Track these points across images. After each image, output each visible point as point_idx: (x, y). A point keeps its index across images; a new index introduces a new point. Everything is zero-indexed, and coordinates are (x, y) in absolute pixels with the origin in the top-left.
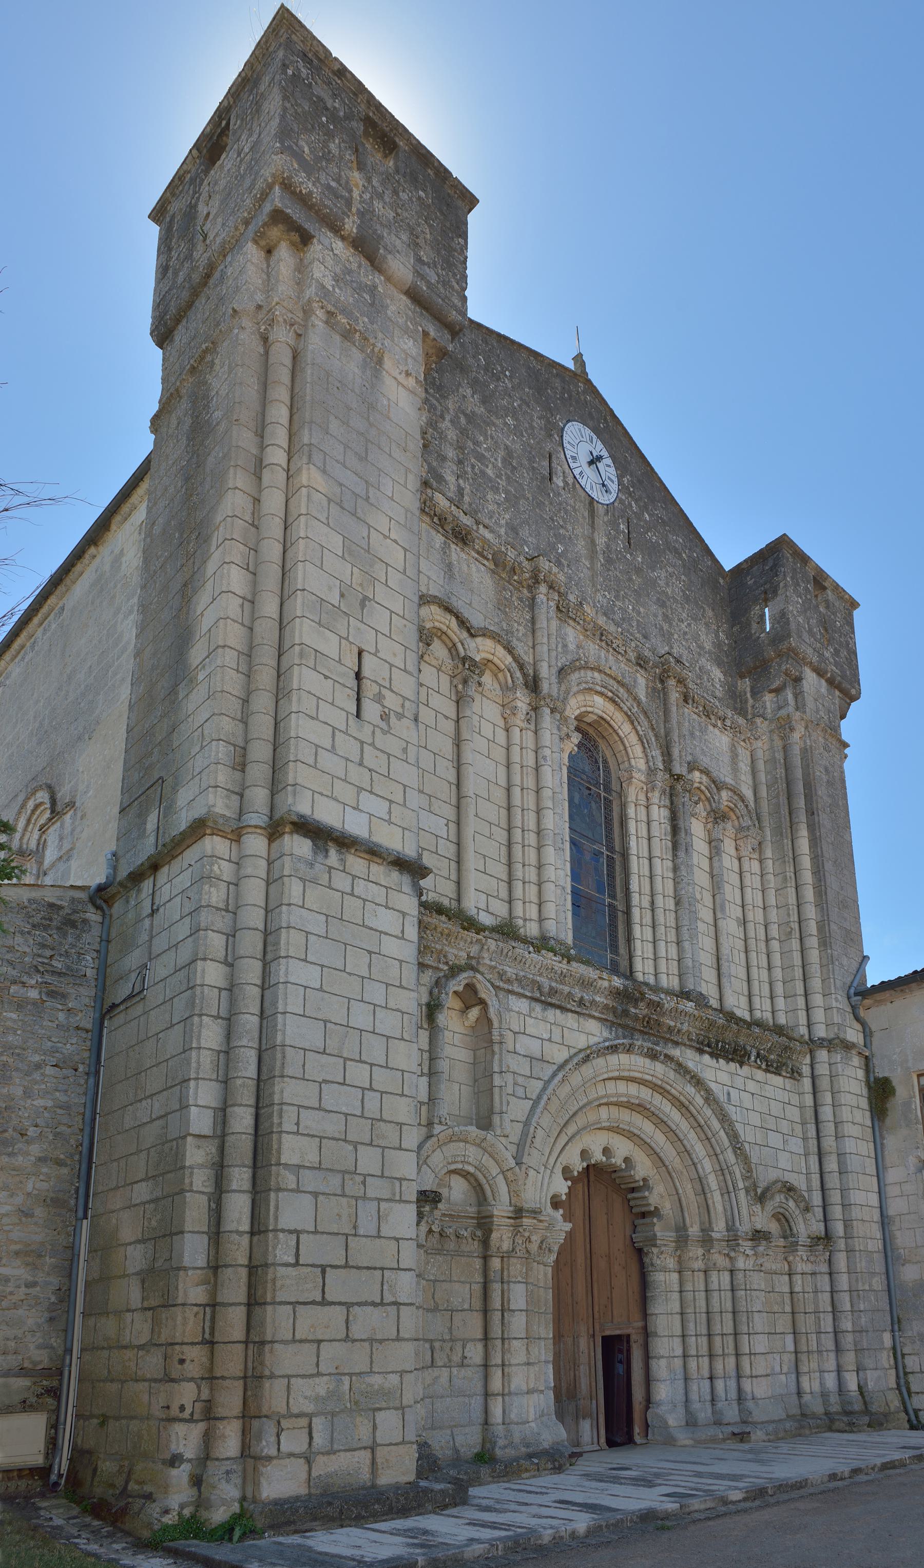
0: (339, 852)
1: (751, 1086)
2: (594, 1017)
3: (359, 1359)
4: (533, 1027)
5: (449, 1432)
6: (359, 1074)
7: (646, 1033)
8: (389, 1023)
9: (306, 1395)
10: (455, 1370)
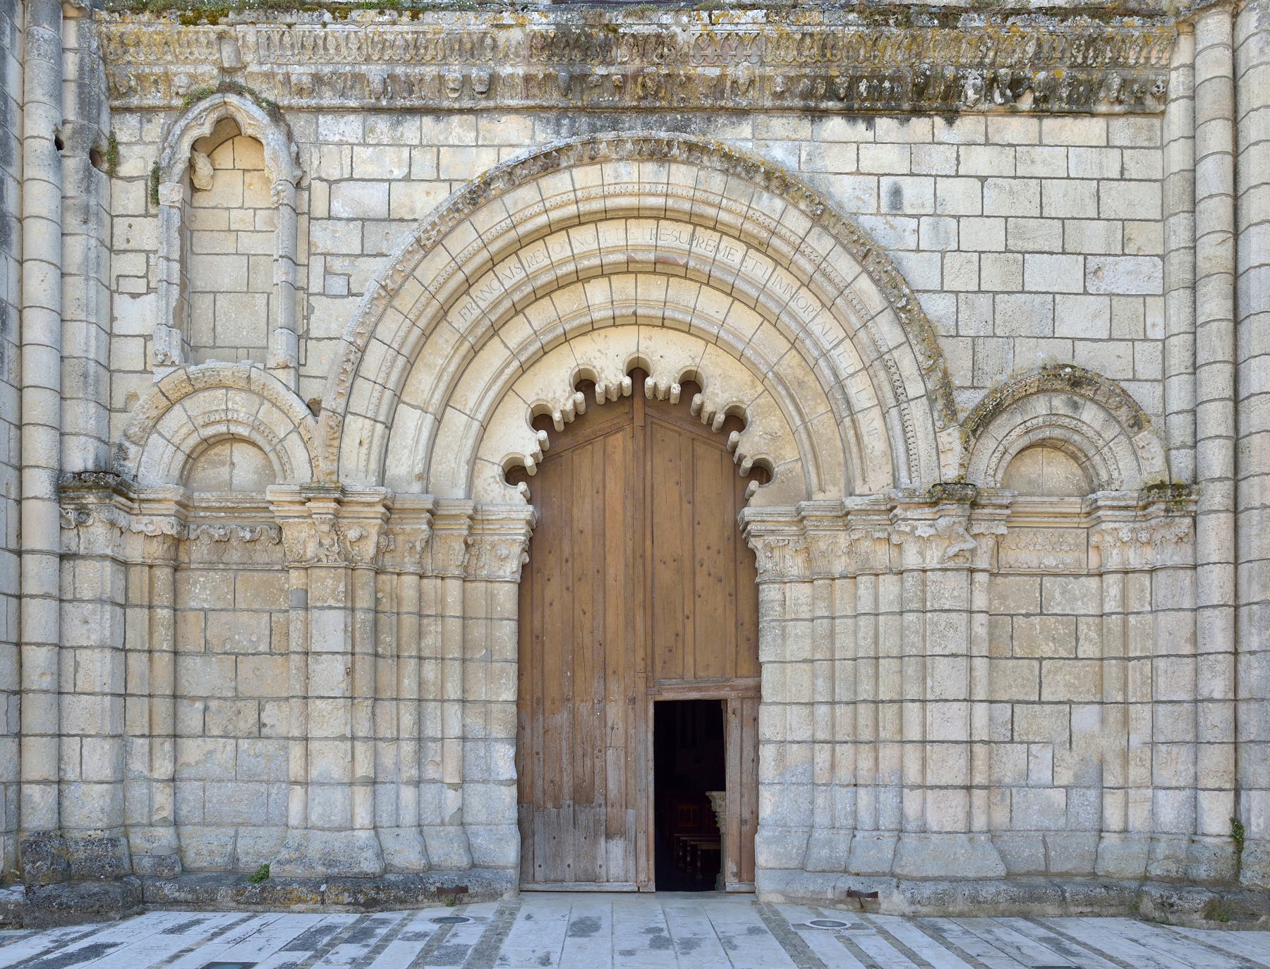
1: (980, 160)
4: (367, 162)
5: (232, 832)
7: (652, 110)
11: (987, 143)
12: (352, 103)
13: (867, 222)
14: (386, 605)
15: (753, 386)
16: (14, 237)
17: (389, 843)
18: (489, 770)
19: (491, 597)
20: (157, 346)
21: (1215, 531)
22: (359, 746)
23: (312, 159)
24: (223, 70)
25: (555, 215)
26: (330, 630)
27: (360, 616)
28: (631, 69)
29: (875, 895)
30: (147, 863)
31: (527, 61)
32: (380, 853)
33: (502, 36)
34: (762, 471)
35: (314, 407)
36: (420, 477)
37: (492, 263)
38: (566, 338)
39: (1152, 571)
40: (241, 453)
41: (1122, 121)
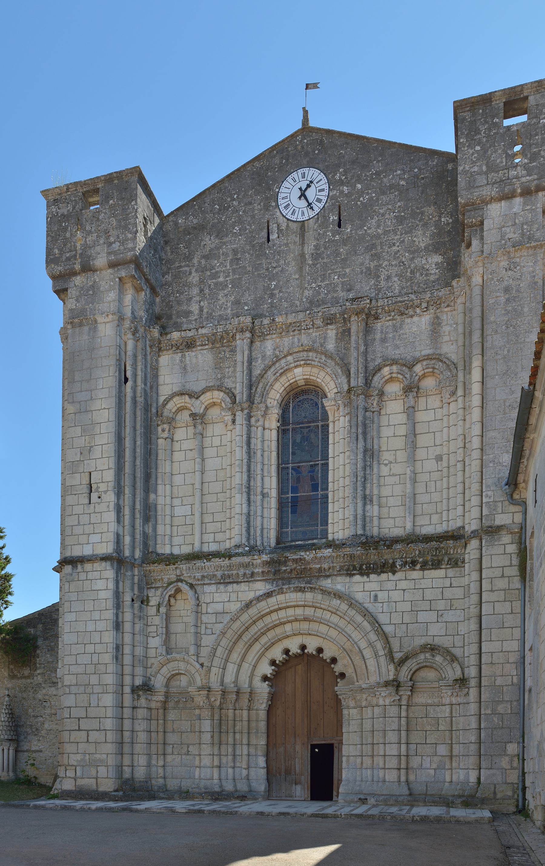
0: (82, 565)
1: (403, 585)
2: (258, 580)
3: (91, 748)
4: (217, 597)
6: (90, 648)
7: (301, 578)
8: (101, 626)
9: (74, 759)
10: (184, 757)
11: (406, 579)
12: (213, 582)
13: (366, 605)
14: (223, 718)
15: (339, 651)
16: (121, 627)
17: (224, 783)
18: (257, 764)
19: (257, 715)
20: (159, 651)
21: (473, 692)
22: (215, 757)
23: (202, 598)
24: (177, 576)
25: (272, 609)
26: (207, 725)
27: (215, 721)
28: (293, 567)
29: (367, 799)
30: (156, 788)
31: (263, 567)
32: (221, 786)
33: (255, 562)
34: (342, 675)
35: (202, 665)
36: (234, 682)
37: (254, 622)
38: (280, 640)
39: (459, 704)
40: (183, 678)
41: (451, 569)
